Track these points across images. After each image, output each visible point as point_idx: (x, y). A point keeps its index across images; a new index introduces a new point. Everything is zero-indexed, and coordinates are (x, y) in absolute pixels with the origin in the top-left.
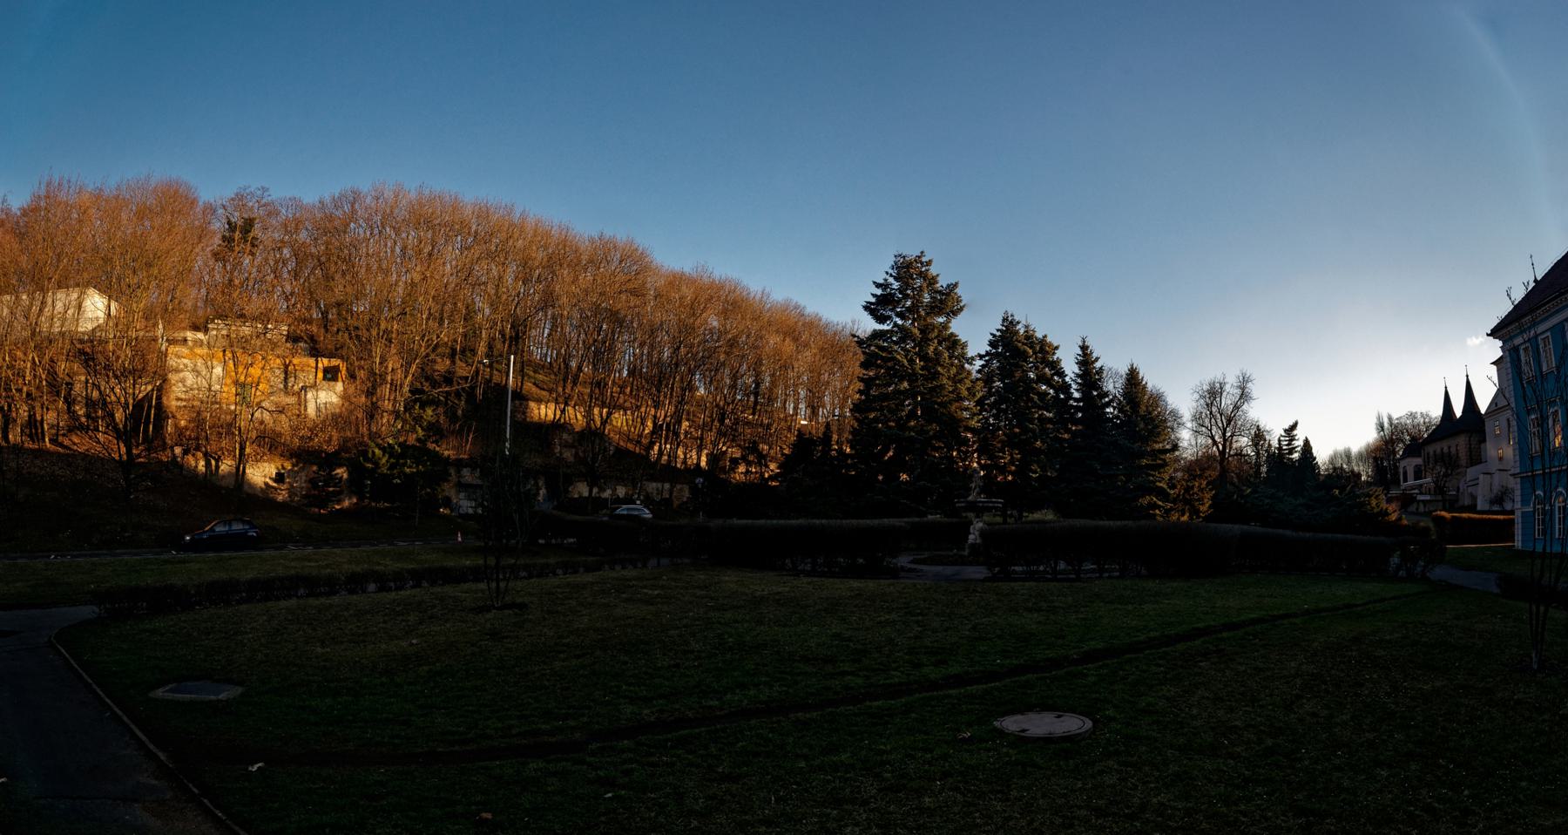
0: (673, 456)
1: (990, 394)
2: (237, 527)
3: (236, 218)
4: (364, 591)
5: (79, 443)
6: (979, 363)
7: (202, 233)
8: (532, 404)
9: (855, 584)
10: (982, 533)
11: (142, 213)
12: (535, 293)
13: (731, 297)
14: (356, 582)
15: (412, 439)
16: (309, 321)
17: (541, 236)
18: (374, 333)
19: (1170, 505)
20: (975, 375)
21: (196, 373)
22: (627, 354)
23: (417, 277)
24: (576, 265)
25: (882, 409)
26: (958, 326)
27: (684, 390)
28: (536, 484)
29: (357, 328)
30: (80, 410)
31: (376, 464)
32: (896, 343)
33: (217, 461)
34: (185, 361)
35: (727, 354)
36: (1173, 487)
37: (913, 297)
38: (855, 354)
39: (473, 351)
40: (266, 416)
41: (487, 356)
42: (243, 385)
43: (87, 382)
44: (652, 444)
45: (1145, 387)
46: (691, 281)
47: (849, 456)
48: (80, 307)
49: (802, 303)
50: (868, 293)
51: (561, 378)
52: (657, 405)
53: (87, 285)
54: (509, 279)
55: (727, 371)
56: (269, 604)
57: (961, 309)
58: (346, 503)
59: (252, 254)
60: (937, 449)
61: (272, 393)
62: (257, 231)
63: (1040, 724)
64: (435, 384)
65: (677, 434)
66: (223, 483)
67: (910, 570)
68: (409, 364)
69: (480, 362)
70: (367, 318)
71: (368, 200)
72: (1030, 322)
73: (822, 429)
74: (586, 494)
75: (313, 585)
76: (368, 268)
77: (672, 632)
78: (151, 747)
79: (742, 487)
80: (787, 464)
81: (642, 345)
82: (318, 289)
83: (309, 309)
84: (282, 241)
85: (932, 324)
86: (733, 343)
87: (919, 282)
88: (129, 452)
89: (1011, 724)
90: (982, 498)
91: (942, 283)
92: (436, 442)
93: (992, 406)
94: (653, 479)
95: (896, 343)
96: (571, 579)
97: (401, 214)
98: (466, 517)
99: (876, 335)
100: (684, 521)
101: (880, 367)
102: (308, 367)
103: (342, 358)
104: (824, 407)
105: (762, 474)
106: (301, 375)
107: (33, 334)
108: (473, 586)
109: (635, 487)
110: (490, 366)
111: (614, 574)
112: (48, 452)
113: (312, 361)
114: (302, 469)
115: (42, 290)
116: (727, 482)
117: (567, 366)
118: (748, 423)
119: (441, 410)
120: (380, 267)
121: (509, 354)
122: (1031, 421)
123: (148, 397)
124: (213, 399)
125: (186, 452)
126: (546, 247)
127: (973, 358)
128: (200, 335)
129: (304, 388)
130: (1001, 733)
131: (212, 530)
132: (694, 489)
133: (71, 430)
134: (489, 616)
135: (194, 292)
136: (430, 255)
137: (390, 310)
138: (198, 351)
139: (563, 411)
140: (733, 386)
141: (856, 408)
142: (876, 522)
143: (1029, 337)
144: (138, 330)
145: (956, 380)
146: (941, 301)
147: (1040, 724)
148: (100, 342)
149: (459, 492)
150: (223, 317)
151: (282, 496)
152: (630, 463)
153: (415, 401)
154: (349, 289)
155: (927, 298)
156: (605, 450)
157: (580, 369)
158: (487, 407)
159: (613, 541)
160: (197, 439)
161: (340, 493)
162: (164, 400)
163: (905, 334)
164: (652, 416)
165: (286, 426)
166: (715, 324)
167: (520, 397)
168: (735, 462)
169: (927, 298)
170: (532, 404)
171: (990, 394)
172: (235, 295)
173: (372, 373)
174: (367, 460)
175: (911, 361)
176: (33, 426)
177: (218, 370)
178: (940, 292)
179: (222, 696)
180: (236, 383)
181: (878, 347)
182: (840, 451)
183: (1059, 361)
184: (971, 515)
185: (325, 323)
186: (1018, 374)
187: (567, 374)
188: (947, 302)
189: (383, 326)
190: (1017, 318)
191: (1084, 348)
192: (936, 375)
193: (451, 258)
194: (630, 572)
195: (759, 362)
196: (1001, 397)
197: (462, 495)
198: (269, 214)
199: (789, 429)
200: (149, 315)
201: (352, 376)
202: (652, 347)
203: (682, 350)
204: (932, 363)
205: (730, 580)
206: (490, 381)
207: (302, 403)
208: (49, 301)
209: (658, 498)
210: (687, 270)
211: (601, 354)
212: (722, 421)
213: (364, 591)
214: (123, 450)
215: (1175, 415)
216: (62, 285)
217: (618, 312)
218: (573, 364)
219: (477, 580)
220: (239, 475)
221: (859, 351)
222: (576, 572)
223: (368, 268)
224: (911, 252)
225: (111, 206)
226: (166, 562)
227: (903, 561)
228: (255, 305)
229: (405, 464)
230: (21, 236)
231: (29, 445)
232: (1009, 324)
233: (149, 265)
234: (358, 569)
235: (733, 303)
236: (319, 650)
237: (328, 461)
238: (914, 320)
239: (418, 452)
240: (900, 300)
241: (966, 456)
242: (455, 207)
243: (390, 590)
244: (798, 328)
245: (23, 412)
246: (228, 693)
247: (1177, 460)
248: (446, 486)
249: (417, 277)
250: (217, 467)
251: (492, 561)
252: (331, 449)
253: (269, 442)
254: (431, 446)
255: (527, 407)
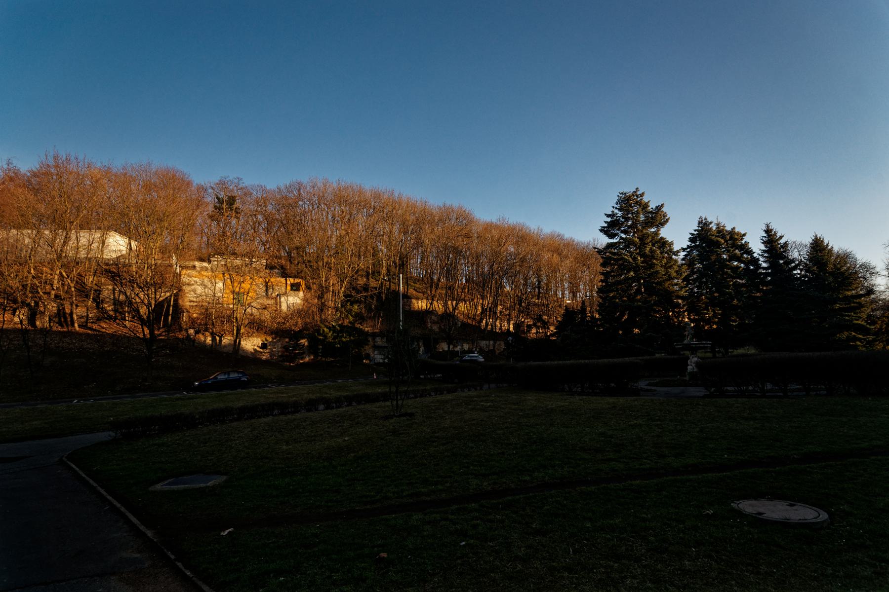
0: (494, 325)
1: (693, 273)
2: (234, 375)
3: (222, 195)
4: (316, 410)
5: (107, 327)
6: (682, 254)
7: (199, 204)
8: (414, 301)
9: (611, 400)
10: (697, 364)
11: (148, 187)
12: (411, 239)
13: (520, 234)
14: (311, 405)
15: (346, 322)
16: (280, 258)
17: (411, 207)
18: (321, 264)
19: (871, 338)
20: (680, 262)
21: (202, 286)
22: (464, 270)
23: (343, 233)
24: (432, 223)
25: (617, 290)
26: (665, 233)
27: (497, 288)
28: (418, 344)
29: (310, 261)
30: (109, 307)
31: (325, 337)
32: (622, 249)
33: (220, 337)
34: (196, 279)
35: (520, 266)
36: (873, 323)
37: (635, 219)
38: (597, 259)
39: (379, 273)
40: (255, 311)
41: (387, 275)
42: (238, 294)
43: (114, 290)
44: (481, 320)
45: (831, 250)
46: (497, 227)
47: (598, 319)
48: (103, 243)
49: (562, 232)
50: (602, 221)
51: (429, 285)
52: (483, 298)
53: (109, 229)
54: (396, 232)
55: (521, 276)
56: (253, 421)
57: (667, 220)
58: (307, 359)
59: (237, 218)
60: (658, 312)
61: (258, 298)
62: (238, 203)
63: (776, 510)
64: (358, 292)
65: (495, 313)
66: (225, 350)
67: (647, 390)
68: (343, 281)
69: (384, 279)
70: (315, 256)
71: (308, 188)
72: (720, 220)
73: (580, 305)
74: (446, 349)
75: (284, 408)
76: (313, 228)
77: (499, 432)
78: (142, 528)
79: (534, 341)
80: (560, 327)
81: (472, 265)
82: (285, 238)
83: (279, 250)
84: (256, 211)
85: (647, 234)
86: (523, 260)
87: (636, 208)
88: (152, 332)
89: (748, 506)
90: (695, 341)
91: (652, 206)
92: (361, 323)
93: (695, 280)
94: (483, 339)
95: (622, 249)
96: (439, 397)
97: (329, 196)
98: (378, 364)
99: (609, 246)
100: (502, 362)
101: (614, 265)
102: (280, 284)
103: (302, 278)
104: (580, 292)
105: (546, 333)
106: (276, 288)
107: (59, 257)
108: (382, 404)
109: (473, 344)
110: (389, 281)
111: (464, 394)
112: (77, 333)
113: (283, 280)
114: (279, 340)
115: (65, 228)
116: (526, 339)
117: (432, 279)
118: (535, 304)
119: (362, 306)
120: (320, 227)
121: (399, 274)
122: (728, 287)
123: (167, 300)
124: (217, 301)
125: (197, 332)
126: (414, 213)
127: (678, 252)
128: (205, 264)
129: (279, 295)
130: (740, 514)
131: (215, 378)
132: (507, 344)
133: (99, 319)
134: (392, 421)
135: (198, 239)
136: (349, 220)
137: (329, 251)
138: (205, 273)
139: (431, 304)
140: (525, 284)
141: (600, 291)
142: (620, 360)
143: (720, 231)
144: (156, 258)
145: (666, 267)
146: (652, 218)
147: (776, 510)
148: (124, 265)
149: (374, 351)
150: (221, 254)
151: (265, 356)
152: (470, 331)
153: (347, 301)
154: (303, 239)
155: (642, 218)
156: (456, 324)
157: (439, 280)
158: (389, 304)
159: (461, 375)
160: (206, 324)
161: (303, 353)
162: (180, 302)
163: (628, 243)
164: (481, 304)
165: (268, 316)
166: (512, 250)
167: (407, 297)
168: (529, 327)
169: (642, 218)
170: (414, 301)
171: (693, 273)
172: (228, 241)
173: (321, 286)
174: (319, 334)
175: (635, 259)
176: (62, 316)
177: (220, 285)
178: (651, 212)
179: (210, 484)
180: (233, 292)
181: (611, 253)
182: (592, 317)
183: (747, 243)
184: (687, 353)
185: (290, 259)
186: (713, 258)
187: (432, 283)
188: (657, 218)
189: (325, 260)
190: (709, 220)
191: (768, 231)
192: (652, 266)
193: (361, 221)
194: (473, 393)
195: (539, 269)
196: (702, 274)
197: (376, 352)
198: (245, 194)
199: (560, 306)
200: (164, 251)
201: (309, 288)
202: (478, 266)
203: (495, 266)
204: (649, 259)
205: (531, 399)
206: (389, 289)
207: (278, 304)
208: (73, 237)
209: (487, 350)
210: (494, 221)
211: (450, 272)
212: (520, 304)
213: (316, 410)
214: (147, 331)
215: (866, 267)
216: (85, 225)
217: (457, 247)
218: (435, 278)
219: (385, 400)
220: (236, 346)
221: (599, 257)
222: (442, 393)
223: (313, 228)
224: (629, 190)
225: (123, 181)
226: (178, 399)
227: (642, 384)
228: (243, 247)
229: (342, 336)
230: (36, 191)
231: (57, 328)
232: (704, 225)
233: (160, 220)
234: (314, 397)
235: (522, 237)
236: (285, 447)
237: (296, 336)
238: (634, 233)
239: (350, 330)
240: (623, 223)
241: (680, 314)
242: (361, 192)
243: (333, 408)
244: (561, 248)
245: (52, 307)
246: (214, 481)
247: (874, 301)
248: (367, 347)
249: (343, 233)
250: (221, 341)
251: (394, 389)
252: (297, 329)
253: (256, 326)
254: (358, 326)
255: (411, 302)
